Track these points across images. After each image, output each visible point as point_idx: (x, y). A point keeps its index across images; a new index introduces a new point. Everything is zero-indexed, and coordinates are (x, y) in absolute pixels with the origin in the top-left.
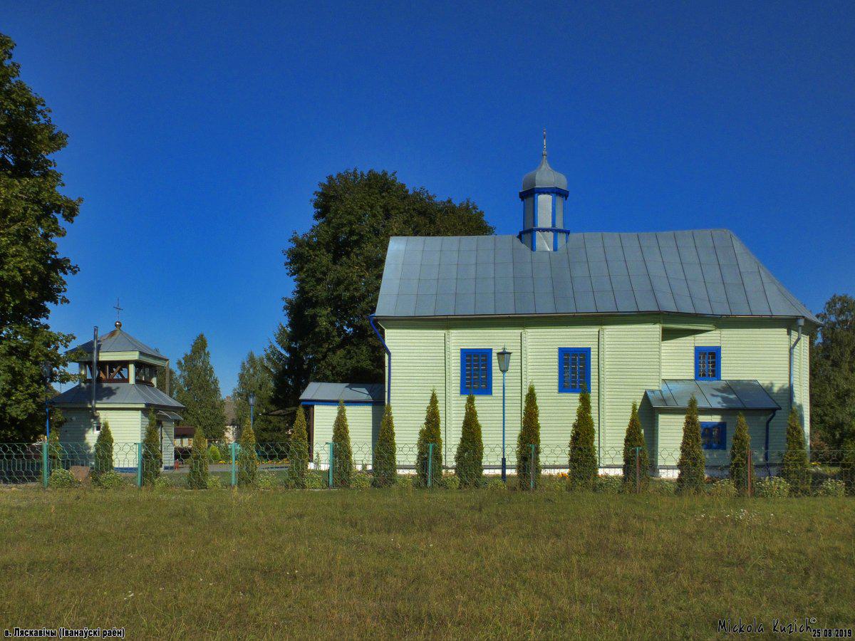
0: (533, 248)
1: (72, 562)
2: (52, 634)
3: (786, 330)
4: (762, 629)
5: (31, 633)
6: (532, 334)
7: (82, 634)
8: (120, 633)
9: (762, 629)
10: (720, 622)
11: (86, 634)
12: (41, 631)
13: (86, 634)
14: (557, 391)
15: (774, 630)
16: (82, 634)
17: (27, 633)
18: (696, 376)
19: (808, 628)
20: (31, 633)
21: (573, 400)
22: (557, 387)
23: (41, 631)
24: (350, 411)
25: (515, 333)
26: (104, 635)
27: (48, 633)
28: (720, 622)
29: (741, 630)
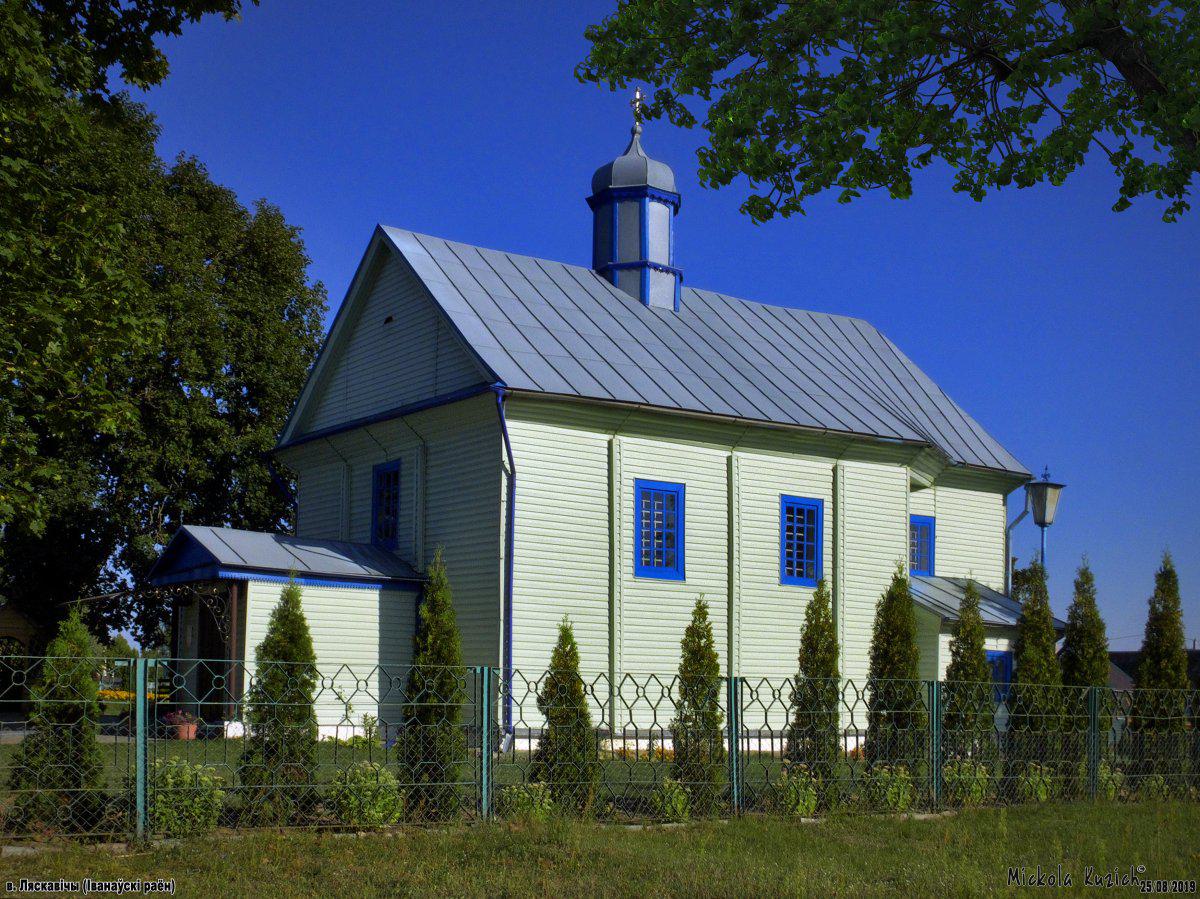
0: (643, 298)
1: (91, 750)
2: (74, 888)
3: (1001, 496)
4: (1069, 881)
5: (44, 886)
6: (750, 461)
7: (115, 888)
8: (169, 886)
9: (1069, 881)
10: (1010, 870)
11: (121, 888)
12: (57, 885)
13: (121, 888)
14: (777, 580)
15: (1087, 882)
16: (115, 888)
17: (38, 887)
18: (242, 585)
19: (1133, 879)
20: (44, 886)
21: (805, 595)
22: (777, 574)
23: (57, 885)
24: (314, 602)
25: (716, 455)
26: (146, 889)
27: (68, 887)
28: (1010, 870)
29: (1039, 883)
